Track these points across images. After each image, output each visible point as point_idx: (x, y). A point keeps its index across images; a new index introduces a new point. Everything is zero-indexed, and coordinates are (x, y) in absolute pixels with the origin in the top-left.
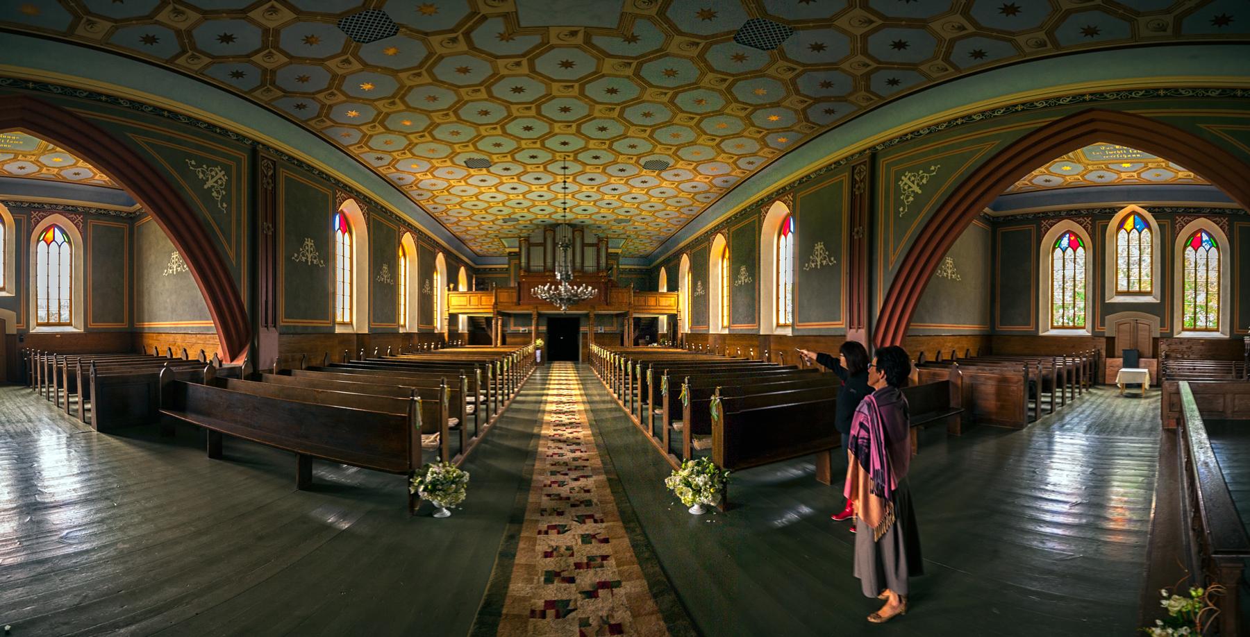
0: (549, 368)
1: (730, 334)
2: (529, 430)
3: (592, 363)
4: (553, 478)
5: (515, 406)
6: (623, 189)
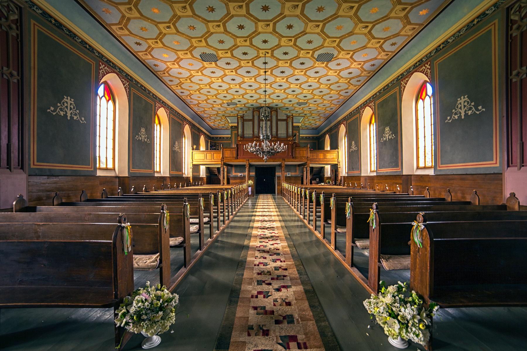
0: (257, 198)
1: (437, 177)
2: (241, 243)
3: (284, 195)
4: (260, 288)
5: (233, 224)
6: (303, 79)
